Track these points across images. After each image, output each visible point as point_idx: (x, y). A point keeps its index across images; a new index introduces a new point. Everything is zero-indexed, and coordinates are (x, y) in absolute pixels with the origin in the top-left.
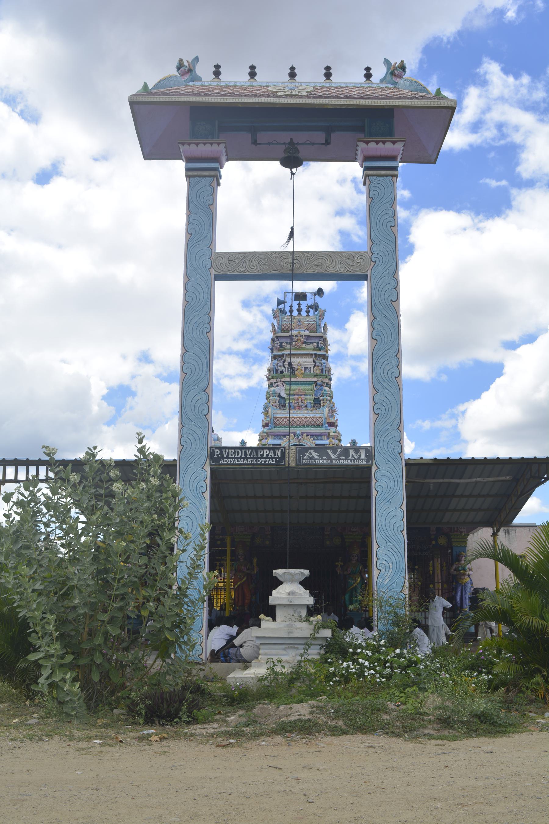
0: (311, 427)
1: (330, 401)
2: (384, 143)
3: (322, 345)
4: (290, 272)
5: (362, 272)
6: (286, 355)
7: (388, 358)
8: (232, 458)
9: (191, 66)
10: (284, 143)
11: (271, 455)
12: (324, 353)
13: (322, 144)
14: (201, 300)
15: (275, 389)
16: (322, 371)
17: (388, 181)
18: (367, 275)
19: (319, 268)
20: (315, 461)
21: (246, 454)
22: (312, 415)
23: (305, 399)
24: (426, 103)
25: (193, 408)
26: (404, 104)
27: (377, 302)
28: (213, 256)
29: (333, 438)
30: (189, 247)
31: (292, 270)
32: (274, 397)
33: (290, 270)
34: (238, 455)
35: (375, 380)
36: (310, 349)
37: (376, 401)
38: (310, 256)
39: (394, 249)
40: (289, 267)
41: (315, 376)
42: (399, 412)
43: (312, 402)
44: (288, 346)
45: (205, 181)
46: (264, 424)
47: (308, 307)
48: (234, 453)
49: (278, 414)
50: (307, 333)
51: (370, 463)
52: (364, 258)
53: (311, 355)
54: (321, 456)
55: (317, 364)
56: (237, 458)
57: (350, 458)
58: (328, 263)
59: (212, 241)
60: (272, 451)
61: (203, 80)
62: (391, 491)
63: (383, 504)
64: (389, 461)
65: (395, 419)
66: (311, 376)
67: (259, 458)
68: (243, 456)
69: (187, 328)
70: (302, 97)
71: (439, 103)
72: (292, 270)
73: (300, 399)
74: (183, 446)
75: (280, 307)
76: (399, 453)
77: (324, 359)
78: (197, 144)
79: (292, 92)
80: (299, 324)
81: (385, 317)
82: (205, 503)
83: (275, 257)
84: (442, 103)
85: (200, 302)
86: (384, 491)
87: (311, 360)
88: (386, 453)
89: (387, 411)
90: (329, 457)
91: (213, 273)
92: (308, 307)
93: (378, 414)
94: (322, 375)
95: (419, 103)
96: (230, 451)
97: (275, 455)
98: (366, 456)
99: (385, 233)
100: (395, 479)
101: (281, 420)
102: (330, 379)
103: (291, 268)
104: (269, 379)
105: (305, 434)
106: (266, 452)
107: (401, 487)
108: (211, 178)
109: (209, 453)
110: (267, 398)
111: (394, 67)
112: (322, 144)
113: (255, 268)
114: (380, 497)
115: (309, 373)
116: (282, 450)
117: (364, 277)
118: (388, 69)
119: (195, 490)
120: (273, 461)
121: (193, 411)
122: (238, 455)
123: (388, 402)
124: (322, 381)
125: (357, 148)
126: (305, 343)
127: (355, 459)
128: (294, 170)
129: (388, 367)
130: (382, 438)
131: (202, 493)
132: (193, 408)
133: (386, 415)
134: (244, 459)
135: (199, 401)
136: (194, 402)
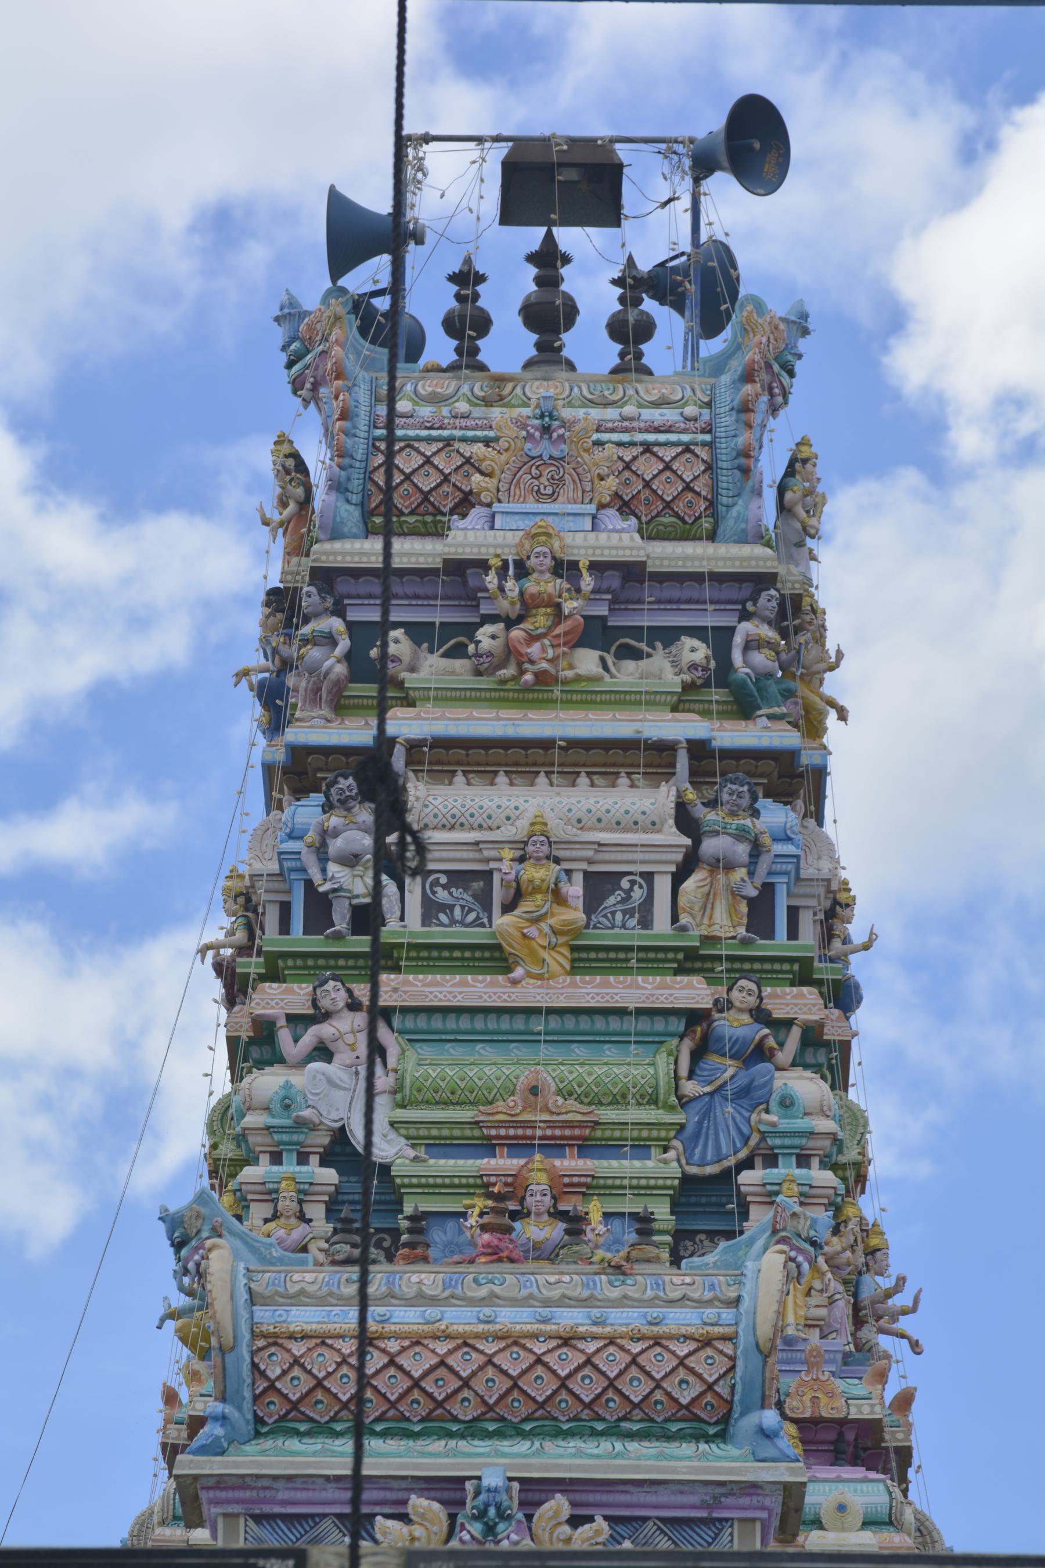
0: (614, 1432)
3: (761, 659)
15: (298, 1079)
16: (759, 912)
22: (624, 1319)
23: (590, 1187)
32: (290, 1167)
36: (646, 699)
41: (690, 961)
43: (661, 1211)
44: (432, 669)
47: (633, 284)
49: (299, 1298)
50: (620, 540)
53: (653, 758)
55: (710, 846)
66: (655, 959)
73: (539, 1183)
77: (782, 795)
80: (545, 448)
87: (658, 800)
92: (633, 284)
94: (763, 947)
102: (844, 996)
104: (235, 989)
105: (559, 1505)
115: (634, 936)
124: (760, 1015)
126: (595, 634)
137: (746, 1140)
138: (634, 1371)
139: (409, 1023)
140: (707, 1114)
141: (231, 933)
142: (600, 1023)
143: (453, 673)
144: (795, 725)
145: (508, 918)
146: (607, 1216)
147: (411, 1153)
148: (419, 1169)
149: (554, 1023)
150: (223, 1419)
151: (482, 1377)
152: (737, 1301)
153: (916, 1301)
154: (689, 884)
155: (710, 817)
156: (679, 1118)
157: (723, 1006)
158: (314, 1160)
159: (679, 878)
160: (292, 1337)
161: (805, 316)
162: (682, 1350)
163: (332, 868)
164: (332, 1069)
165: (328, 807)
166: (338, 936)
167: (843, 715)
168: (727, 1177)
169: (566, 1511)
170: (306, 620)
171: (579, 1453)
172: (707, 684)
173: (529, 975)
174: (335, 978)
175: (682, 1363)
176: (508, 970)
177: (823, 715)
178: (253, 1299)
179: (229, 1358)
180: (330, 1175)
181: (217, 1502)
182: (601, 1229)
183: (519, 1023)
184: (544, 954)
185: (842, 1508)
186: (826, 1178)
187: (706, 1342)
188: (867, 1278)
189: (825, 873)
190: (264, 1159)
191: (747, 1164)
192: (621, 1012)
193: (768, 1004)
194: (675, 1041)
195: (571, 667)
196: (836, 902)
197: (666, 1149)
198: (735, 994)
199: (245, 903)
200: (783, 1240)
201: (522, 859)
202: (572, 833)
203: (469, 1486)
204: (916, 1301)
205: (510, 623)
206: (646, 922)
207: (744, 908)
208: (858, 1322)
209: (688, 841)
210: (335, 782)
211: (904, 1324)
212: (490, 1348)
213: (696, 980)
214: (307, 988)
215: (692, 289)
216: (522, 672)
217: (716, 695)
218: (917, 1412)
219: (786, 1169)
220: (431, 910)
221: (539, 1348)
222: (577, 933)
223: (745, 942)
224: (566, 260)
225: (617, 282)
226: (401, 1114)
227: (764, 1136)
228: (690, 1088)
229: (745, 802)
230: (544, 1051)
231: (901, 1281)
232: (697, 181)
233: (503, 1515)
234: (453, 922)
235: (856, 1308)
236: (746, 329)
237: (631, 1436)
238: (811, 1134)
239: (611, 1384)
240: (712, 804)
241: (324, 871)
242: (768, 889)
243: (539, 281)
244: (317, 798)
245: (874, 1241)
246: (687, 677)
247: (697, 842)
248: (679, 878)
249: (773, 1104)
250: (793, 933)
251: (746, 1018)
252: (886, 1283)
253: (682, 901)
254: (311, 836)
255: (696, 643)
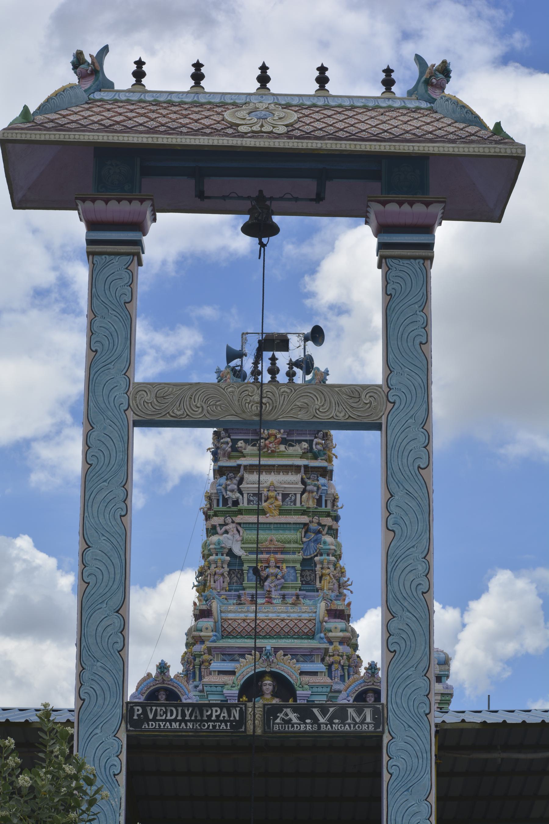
0: (292, 638)
1: (335, 565)
2: (411, 204)
3: (319, 447)
4: (257, 418)
5: (373, 419)
6: (245, 467)
7: (412, 561)
8: (162, 721)
9: (97, 65)
10: (249, 198)
11: (224, 717)
12: (324, 464)
13: (311, 200)
14: (112, 462)
15: (221, 538)
16: (319, 502)
17: (417, 267)
18: (381, 424)
19: (303, 411)
20: (293, 726)
21: (183, 715)
22: (294, 616)
23: (284, 561)
24: (476, 150)
25: (99, 640)
26: (441, 151)
27: (396, 469)
28: (131, 389)
29: (341, 643)
30: (93, 373)
31: (260, 415)
32: (219, 556)
33: (256, 415)
34: (171, 715)
35: (390, 596)
36: (294, 455)
37: (392, 631)
38: (289, 391)
39: (425, 382)
40: (255, 409)
41: (304, 512)
42: (427, 649)
43: (298, 566)
44: (249, 449)
45: (118, 262)
46: (197, 612)
47: (292, 364)
48: (165, 713)
49: (230, 612)
51: (381, 729)
52: (376, 396)
53: (296, 469)
54: (302, 719)
55: (308, 488)
56: (170, 721)
57: (349, 721)
58: (318, 403)
59: (130, 364)
60: (225, 710)
61: (116, 88)
62: (412, 774)
63: (399, 793)
64: (410, 726)
65: (421, 660)
66: (297, 512)
67: (205, 721)
68: (179, 718)
69: (90, 509)
70: (279, 136)
71: (497, 150)
72: (260, 415)
73: (272, 561)
74: (84, 700)
75: (233, 364)
76: (426, 715)
77: (324, 476)
78: (107, 201)
79: (262, 126)
81: (408, 493)
82: (118, 791)
83: (233, 392)
84: (503, 151)
85: (110, 466)
86: (402, 774)
87: (297, 478)
88: (405, 714)
89: (408, 647)
90: (315, 720)
91: (131, 417)
92: (292, 364)
93: (395, 651)
94: (320, 509)
95: (466, 150)
96: (159, 709)
97: (230, 716)
98: (374, 718)
99: (410, 354)
100: (419, 754)
101: (235, 625)
102: (336, 519)
103: (258, 412)
104: (208, 517)
105: (281, 652)
106: (216, 711)
107: (429, 768)
108: (129, 257)
109: (125, 711)
110: (205, 557)
111: (431, 73)
112: (311, 200)
113: (200, 410)
114: (395, 784)
115: (293, 507)
116: (241, 708)
117: (377, 427)
118: (422, 73)
119: (103, 770)
120: (226, 726)
121: (100, 645)
122: (171, 715)
123: (410, 632)
125: (368, 209)
126: (284, 441)
127: (356, 723)
128: (265, 240)
129: (411, 576)
130: (400, 690)
131: (115, 775)
132: (99, 640)
133: (406, 653)
134: (180, 722)
135: (109, 629)
136: (100, 629)
137: (316, 551)
138: (296, 626)
139: (245, 526)
140: (308, 545)
141: (206, 505)
142: (285, 526)
143: (254, 450)
144: (326, 461)
145: (266, 504)
146: (287, 567)
147: (245, 554)
148: (247, 557)
149: (275, 526)
150: (216, 636)
151: (266, 627)
152: (316, 612)
153: (352, 583)
154: (304, 496)
155: (309, 481)
156: (302, 546)
157: (311, 522)
158: (225, 555)
159: (302, 494)
160: (229, 619)
161: (328, 371)
162: (305, 622)
163: (228, 492)
164: (228, 536)
165: (227, 479)
166: (229, 507)
167: (336, 458)
168: (312, 559)
169: (283, 653)
170: (222, 439)
171: (285, 642)
172: (308, 452)
173: (270, 516)
174: (229, 516)
175: (305, 624)
176: (265, 514)
177: (332, 458)
178: (221, 612)
179: (217, 624)
180: (228, 558)
181: (215, 651)
182: (286, 570)
183: (268, 526)
184: (273, 511)
185: (336, 628)
186: (333, 558)
187: (310, 620)
188: (341, 578)
189: (333, 492)
190: (214, 555)
191: (316, 556)
192: (290, 524)
193: (321, 522)
194: (301, 530)
195: (279, 449)
196: (335, 498)
197: (299, 553)
198: (314, 520)
199: (209, 498)
200: (325, 600)
201: (268, 491)
202: (279, 485)
203: (264, 649)
204: (352, 583)
205: (266, 439)
206: (295, 504)
207: (316, 501)
208: (340, 588)
209: (304, 487)
210: (228, 474)
211: (349, 587)
212: (268, 622)
213: (305, 517)
214: (223, 518)
215: (304, 365)
216: (268, 450)
217: (310, 455)
218: (352, 606)
219: (325, 557)
220: (249, 501)
221: (277, 622)
222: (280, 507)
223: (316, 508)
224: (277, 359)
225: (288, 364)
226: (243, 546)
227: (320, 550)
228: (305, 540)
229: (316, 478)
230: (273, 532)
231: (349, 579)
232: (305, 343)
233: (270, 654)
234: (254, 504)
235: (339, 585)
236: (315, 375)
237: (295, 638)
238: (330, 549)
239: (291, 629)
240: (309, 478)
241: (226, 493)
242: (321, 497)
243: (271, 364)
244: (225, 477)
245: (343, 570)
246: (303, 451)
247: (306, 487)
248: (302, 494)
249: (322, 543)
250: (326, 506)
251: (316, 525)
252: (345, 579)
253: (302, 500)
254: (224, 486)
255: (305, 443)
